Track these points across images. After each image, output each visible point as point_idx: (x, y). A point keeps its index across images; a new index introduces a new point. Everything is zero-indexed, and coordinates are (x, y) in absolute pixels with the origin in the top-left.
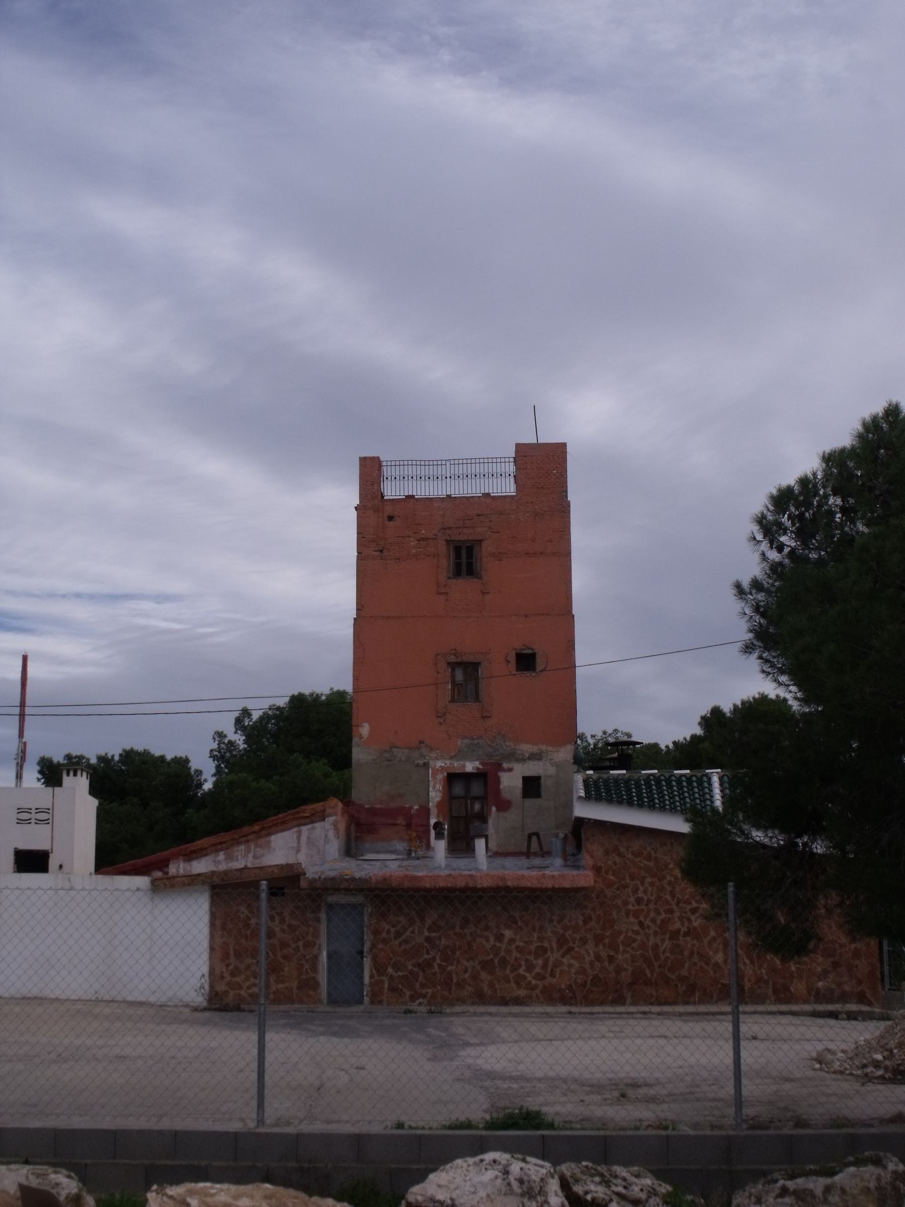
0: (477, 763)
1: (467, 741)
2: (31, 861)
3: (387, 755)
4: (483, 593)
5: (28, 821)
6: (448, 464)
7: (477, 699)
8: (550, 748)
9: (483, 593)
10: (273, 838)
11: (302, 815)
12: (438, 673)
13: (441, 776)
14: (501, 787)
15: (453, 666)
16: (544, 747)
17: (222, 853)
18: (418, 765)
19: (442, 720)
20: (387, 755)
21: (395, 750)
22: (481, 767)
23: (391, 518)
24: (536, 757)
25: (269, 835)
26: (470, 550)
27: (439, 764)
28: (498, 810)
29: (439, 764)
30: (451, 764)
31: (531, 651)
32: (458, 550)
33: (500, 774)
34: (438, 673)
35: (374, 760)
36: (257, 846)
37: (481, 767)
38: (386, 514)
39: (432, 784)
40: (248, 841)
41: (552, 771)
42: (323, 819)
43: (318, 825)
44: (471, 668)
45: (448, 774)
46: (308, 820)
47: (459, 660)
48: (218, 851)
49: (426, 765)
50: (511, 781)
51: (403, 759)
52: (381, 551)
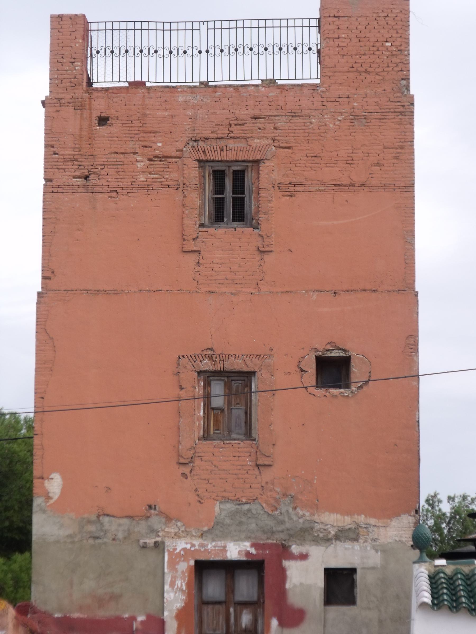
1: (230, 506)
3: (92, 528)
6: (204, 28)
8: (372, 521)
13: (185, 566)
15: (208, 376)
16: (362, 519)
18: (145, 546)
19: (186, 470)
20: (92, 528)
21: (106, 520)
22: (253, 551)
24: (344, 535)
26: (239, 176)
27: (181, 545)
28: (282, 624)
29: (181, 545)
30: (202, 545)
31: (342, 354)
33: (286, 563)
35: (70, 536)
37: (253, 551)
38: (95, 114)
39: (168, 579)
41: (375, 559)
44: (239, 381)
50: (304, 577)
51: (120, 536)
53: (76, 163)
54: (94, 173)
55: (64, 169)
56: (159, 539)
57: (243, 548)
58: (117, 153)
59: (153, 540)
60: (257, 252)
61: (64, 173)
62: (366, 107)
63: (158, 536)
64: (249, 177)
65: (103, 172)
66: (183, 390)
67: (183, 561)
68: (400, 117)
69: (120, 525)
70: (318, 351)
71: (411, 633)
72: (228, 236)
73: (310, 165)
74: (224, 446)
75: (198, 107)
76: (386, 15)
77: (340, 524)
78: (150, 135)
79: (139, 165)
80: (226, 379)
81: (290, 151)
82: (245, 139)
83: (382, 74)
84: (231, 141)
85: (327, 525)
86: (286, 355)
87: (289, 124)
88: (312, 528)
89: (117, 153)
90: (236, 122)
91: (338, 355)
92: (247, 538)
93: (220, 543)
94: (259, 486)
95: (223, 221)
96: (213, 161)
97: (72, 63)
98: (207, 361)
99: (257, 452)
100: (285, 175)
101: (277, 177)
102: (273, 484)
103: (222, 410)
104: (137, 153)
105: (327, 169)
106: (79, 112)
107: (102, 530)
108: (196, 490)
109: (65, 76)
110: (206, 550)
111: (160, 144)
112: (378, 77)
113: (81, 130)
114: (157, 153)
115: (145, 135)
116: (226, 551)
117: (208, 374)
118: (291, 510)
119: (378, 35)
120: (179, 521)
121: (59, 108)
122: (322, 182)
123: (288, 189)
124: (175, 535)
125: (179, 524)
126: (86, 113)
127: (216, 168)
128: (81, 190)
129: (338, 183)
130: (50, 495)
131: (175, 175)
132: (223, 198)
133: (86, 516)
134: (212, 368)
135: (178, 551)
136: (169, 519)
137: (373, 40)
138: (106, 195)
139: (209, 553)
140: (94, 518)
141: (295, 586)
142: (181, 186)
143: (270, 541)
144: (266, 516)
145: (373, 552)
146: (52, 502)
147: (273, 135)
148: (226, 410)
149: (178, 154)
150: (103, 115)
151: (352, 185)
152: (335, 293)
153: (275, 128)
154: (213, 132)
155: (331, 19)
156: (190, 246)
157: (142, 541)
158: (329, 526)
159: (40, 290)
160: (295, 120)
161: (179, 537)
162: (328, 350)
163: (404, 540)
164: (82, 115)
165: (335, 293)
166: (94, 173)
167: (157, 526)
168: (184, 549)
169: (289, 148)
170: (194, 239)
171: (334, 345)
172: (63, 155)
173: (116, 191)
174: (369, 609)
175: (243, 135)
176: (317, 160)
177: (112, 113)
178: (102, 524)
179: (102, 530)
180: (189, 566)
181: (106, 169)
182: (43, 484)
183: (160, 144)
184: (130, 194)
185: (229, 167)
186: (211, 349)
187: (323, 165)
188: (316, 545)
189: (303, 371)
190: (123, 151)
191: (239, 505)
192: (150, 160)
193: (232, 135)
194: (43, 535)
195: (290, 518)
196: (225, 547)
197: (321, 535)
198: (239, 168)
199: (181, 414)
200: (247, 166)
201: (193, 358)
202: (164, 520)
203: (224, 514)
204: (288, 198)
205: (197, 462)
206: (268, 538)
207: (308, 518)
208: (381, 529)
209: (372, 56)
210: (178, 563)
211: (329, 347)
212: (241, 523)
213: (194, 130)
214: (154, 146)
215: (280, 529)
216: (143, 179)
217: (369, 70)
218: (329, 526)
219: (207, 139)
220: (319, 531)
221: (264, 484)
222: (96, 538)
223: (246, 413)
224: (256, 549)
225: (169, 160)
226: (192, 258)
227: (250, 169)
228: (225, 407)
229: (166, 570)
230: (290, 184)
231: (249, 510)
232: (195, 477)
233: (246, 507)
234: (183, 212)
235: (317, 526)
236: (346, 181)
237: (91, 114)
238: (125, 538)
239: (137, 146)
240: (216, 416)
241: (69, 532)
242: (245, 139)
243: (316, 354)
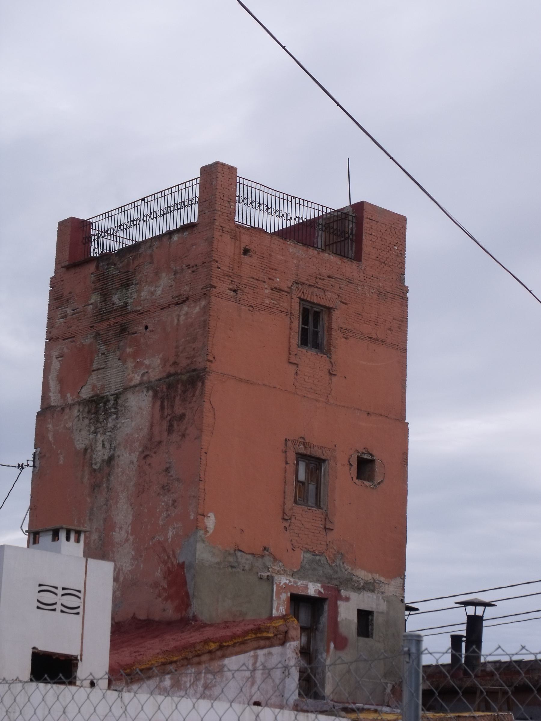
0: (319, 585)
1: (308, 555)
2: (52, 668)
3: (231, 559)
4: (331, 374)
5: (50, 606)
6: (294, 201)
7: (318, 504)
8: (382, 579)
9: (331, 374)
10: (227, 661)
11: (265, 634)
12: (287, 463)
13: (285, 596)
14: (339, 619)
15: (301, 456)
16: (377, 576)
17: (168, 677)
18: (261, 578)
19: (287, 525)
20: (231, 559)
21: (239, 554)
22: (322, 591)
23: (246, 251)
24: (369, 587)
25: (224, 656)
26: (317, 315)
27: (284, 580)
28: (336, 647)
29: (284, 580)
30: (295, 582)
31: (369, 458)
32: (305, 313)
33: (339, 603)
34: (287, 463)
35: (218, 563)
36: (208, 672)
37: (322, 591)
38: (243, 246)
39: (275, 605)
40: (199, 663)
41: (383, 607)
42: (283, 643)
43: (276, 650)
44: (315, 463)
45: (292, 595)
46: (267, 642)
47: (308, 452)
48: (165, 673)
49: (270, 580)
50: (347, 613)
51: (247, 567)
52: (235, 291)
53: (230, 278)
54: (241, 289)
55: (223, 281)
56: (269, 574)
57: (317, 588)
58: (253, 278)
59: (266, 574)
60: (328, 374)
61: (223, 284)
62: (386, 288)
63: (269, 571)
64: (324, 318)
66: (288, 465)
67: (284, 592)
68: (401, 300)
69: (247, 559)
70: (358, 452)
72: (308, 356)
74: (308, 510)
75: (300, 259)
77: (366, 579)
78: (273, 271)
80: (307, 461)
82: (324, 290)
83: (392, 267)
84: (316, 289)
85: (359, 578)
86: (343, 451)
87: (346, 287)
88: (352, 579)
89: (253, 278)
90: (320, 277)
92: (318, 581)
93: (305, 582)
94: (325, 544)
95: (307, 346)
97: (229, 202)
99: (326, 519)
102: (333, 543)
104: (265, 282)
105: (365, 325)
106: (233, 240)
107: (237, 562)
108: (291, 541)
109: (225, 211)
110: (297, 586)
111: (278, 280)
112: (390, 269)
113: (234, 254)
114: (276, 285)
115: (270, 270)
116: (308, 588)
118: (341, 564)
119: (391, 239)
120: (281, 562)
121: (222, 234)
122: (362, 333)
123: (346, 333)
124: (278, 572)
125: (281, 564)
128: (233, 300)
129: (371, 336)
130: (208, 529)
131: (286, 305)
132: (308, 329)
133: (228, 549)
135: (282, 584)
136: (275, 559)
137: (388, 242)
138: (247, 308)
139: (299, 588)
140: (232, 552)
141: (343, 620)
142: (289, 314)
143: (329, 585)
144: (328, 566)
145: (382, 601)
146: (208, 534)
147: (338, 292)
148: (306, 484)
149: (288, 290)
150: (247, 247)
151: (377, 340)
152: (368, 414)
153: (340, 288)
154: (308, 280)
156: (293, 360)
157: (260, 574)
158: (360, 579)
160: (350, 285)
161: (281, 574)
162: (363, 453)
163: (397, 595)
164: (235, 243)
165: (368, 414)
166: (241, 289)
167: (269, 564)
168: (285, 584)
172: (223, 270)
173: (252, 306)
174: (379, 642)
175: (322, 287)
177: (252, 247)
178: (237, 557)
179: (237, 562)
180: (287, 596)
181: (247, 289)
182: (203, 520)
183: (278, 280)
187: (363, 322)
188: (354, 592)
190: (257, 278)
191: (314, 555)
192: (272, 289)
193: (317, 285)
194: (202, 560)
195: (341, 570)
196: (307, 585)
197: (356, 585)
198: (317, 310)
199: (287, 482)
200: (322, 310)
201: (294, 442)
202: (272, 560)
203: (306, 560)
205: (293, 520)
206: (329, 583)
207: (350, 571)
208: (387, 586)
209: (388, 253)
210: (281, 594)
212: (314, 569)
213: (297, 275)
214: (275, 280)
215: (335, 577)
216: (267, 302)
218: (360, 579)
219: (304, 284)
220: (354, 581)
221: (328, 543)
222: (232, 567)
223: (317, 488)
224: (324, 590)
225: (283, 293)
226: (293, 368)
227: (324, 313)
228: (306, 482)
229: (274, 598)
231: (320, 560)
232: (292, 531)
233: (318, 558)
234: (290, 334)
235: (355, 578)
236: (375, 337)
237: (240, 245)
238: (250, 570)
239: (265, 277)
241: (218, 560)
242: (324, 290)
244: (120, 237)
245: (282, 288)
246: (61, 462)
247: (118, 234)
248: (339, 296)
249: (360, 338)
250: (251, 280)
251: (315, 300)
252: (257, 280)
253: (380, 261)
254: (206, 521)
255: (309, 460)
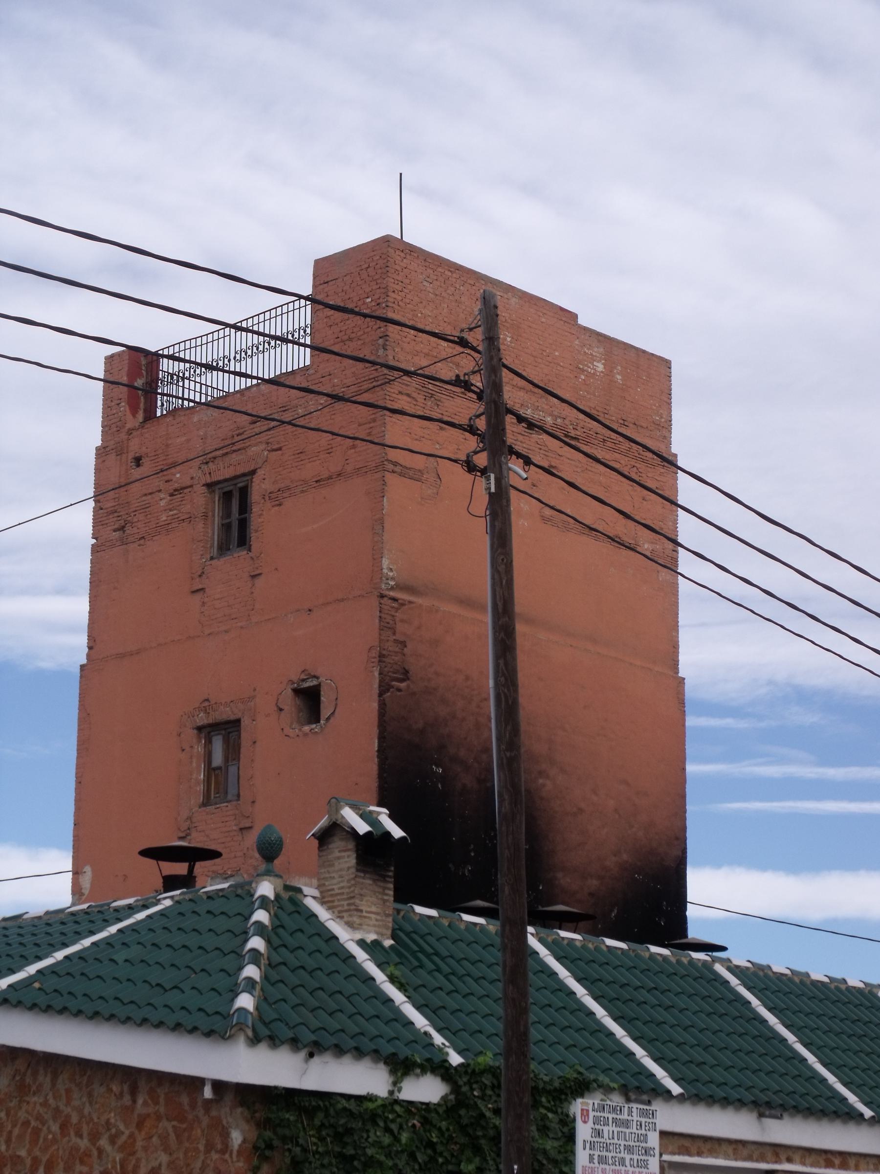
31: (315, 683)
38: (131, 455)
62: (345, 381)
65: (135, 520)
71: (859, 969)
73: (297, 464)
76: (366, 266)
79: (162, 503)
80: (223, 732)
81: (279, 452)
86: (267, 693)
89: (146, 495)
91: (312, 684)
96: (219, 482)
98: (202, 714)
100: (275, 482)
101: (268, 486)
103: (219, 768)
112: (360, 342)
117: (209, 729)
123: (276, 498)
126: (124, 456)
127: (226, 489)
128: (118, 543)
130: (83, 891)
134: (206, 722)
138: (136, 545)
150: (137, 455)
155: (321, 287)
159: (85, 661)
162: (303, 680)
169: (280, 449)
170: (200, 576)
171: (306, 673)
176: (302, 456)
184: (154, 538)
185: (236, 484)
186: (207, 700)
189: (281, 710)
204: (276, 508)
211: (303, 677)
216: (164, 518)
217: (353, 335)
230: (279, 490)
236: (325, 475)
240: (216, 776)
243: (292, 686)
244: (201, 384)
245: (184, 485)
246: (451, 865)
247: (198, 379)
248: (268, 443)
249: (302, 492)
250: (144, 498)
251: (228, 473)
252: (151, 494)
253: (342, 341)
254: (80, 880)
255: (225, 729)
